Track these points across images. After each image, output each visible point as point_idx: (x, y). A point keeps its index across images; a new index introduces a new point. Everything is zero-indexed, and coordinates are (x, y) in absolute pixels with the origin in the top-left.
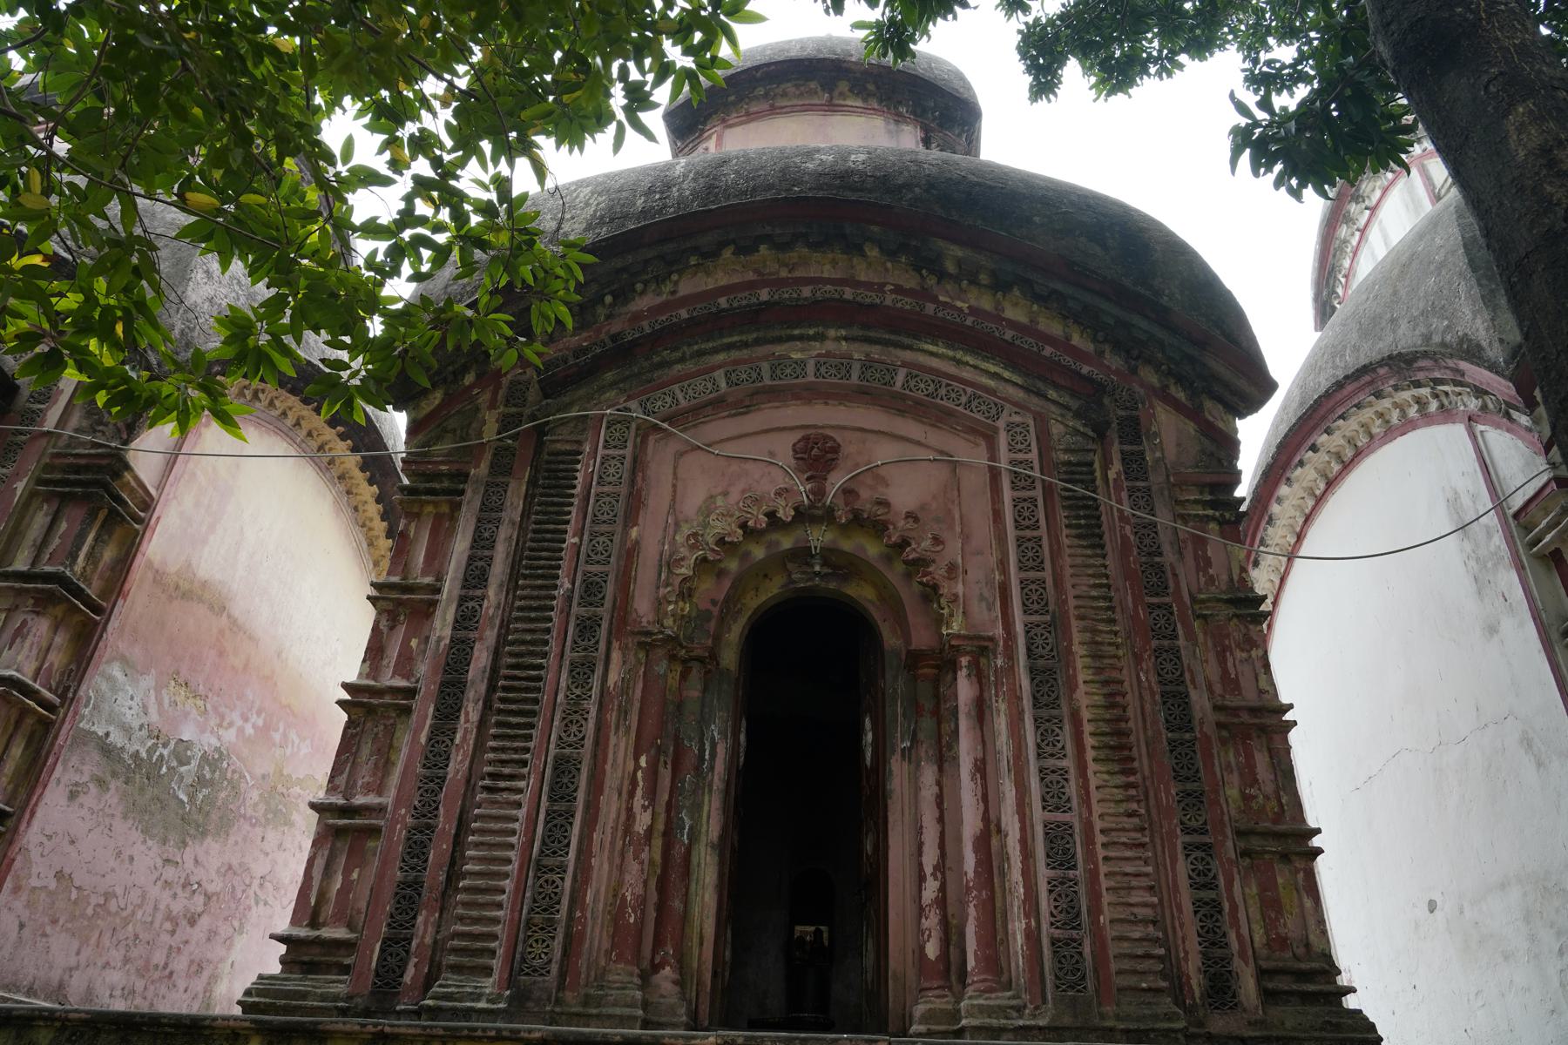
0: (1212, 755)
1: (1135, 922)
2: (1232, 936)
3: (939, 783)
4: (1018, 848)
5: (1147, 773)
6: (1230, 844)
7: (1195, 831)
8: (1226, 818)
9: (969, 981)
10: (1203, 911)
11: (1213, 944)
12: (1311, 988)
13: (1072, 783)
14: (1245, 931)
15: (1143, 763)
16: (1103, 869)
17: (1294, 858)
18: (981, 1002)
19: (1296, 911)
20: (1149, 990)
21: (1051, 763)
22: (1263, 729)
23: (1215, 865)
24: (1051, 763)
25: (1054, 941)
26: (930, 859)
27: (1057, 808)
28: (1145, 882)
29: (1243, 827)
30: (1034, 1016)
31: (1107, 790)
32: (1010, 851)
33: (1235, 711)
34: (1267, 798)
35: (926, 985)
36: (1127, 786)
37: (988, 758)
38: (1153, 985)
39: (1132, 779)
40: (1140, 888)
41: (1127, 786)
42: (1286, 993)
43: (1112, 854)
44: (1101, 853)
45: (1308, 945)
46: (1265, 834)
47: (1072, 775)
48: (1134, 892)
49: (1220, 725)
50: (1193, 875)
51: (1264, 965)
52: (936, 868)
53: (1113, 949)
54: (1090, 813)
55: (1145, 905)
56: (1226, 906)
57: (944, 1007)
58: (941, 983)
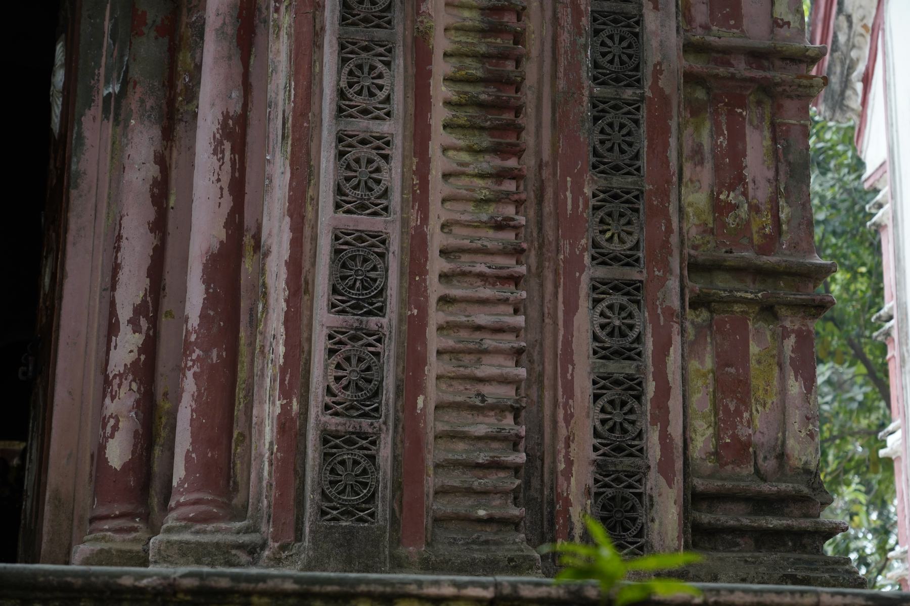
0: (667, 131)
1: (479, 409)
2: (653, 438)
3: (162, 161)
4: (284, 275)
5: (546, 156)
6: (673, 284)
7: (616, 259)
8: (674, 239)
9: (172, 503)
10: (609, 395)
11: (619, 449)
12: (774, 522)
13: (396, 164)
14: (676, 429)
15: (538, 135)
16: (436, 317)
17: (783, 312)
18: (187, 536)
19: (773, 399)
20: (489, 520)
21: (361, 125)
22: (768, 91)
23: (643, 320)
24: (361, 125)
25: (326, 437)
26: (131, 291)
27: (362, 207)
28: (508, 341)
29: (701, 256)
30: (277, 561)
31: (465, 181)
32: (270, 280)
33: (724, 54)
34: (755, 209)
35: (102, 511)
36: (500, 175)
37: (253, 116)
38: (497, 513)
39: (512, 163)
40: (497, 352)
41: (500, 175)
42: (732, 530)
43: (456, 292)
44: (435, 289)
45: (782, 456)
46: (740, 271)
47: (396, 152)
48: (486, 359)
49: (691, 78)
50: (602, 334)
51: (700, 484)
52: (139, 310)
53: (433, 454)
54: (425, 219)
55: (504, 380)
56: (651, 388)
57: (127, 547)
58: (127, 508)
